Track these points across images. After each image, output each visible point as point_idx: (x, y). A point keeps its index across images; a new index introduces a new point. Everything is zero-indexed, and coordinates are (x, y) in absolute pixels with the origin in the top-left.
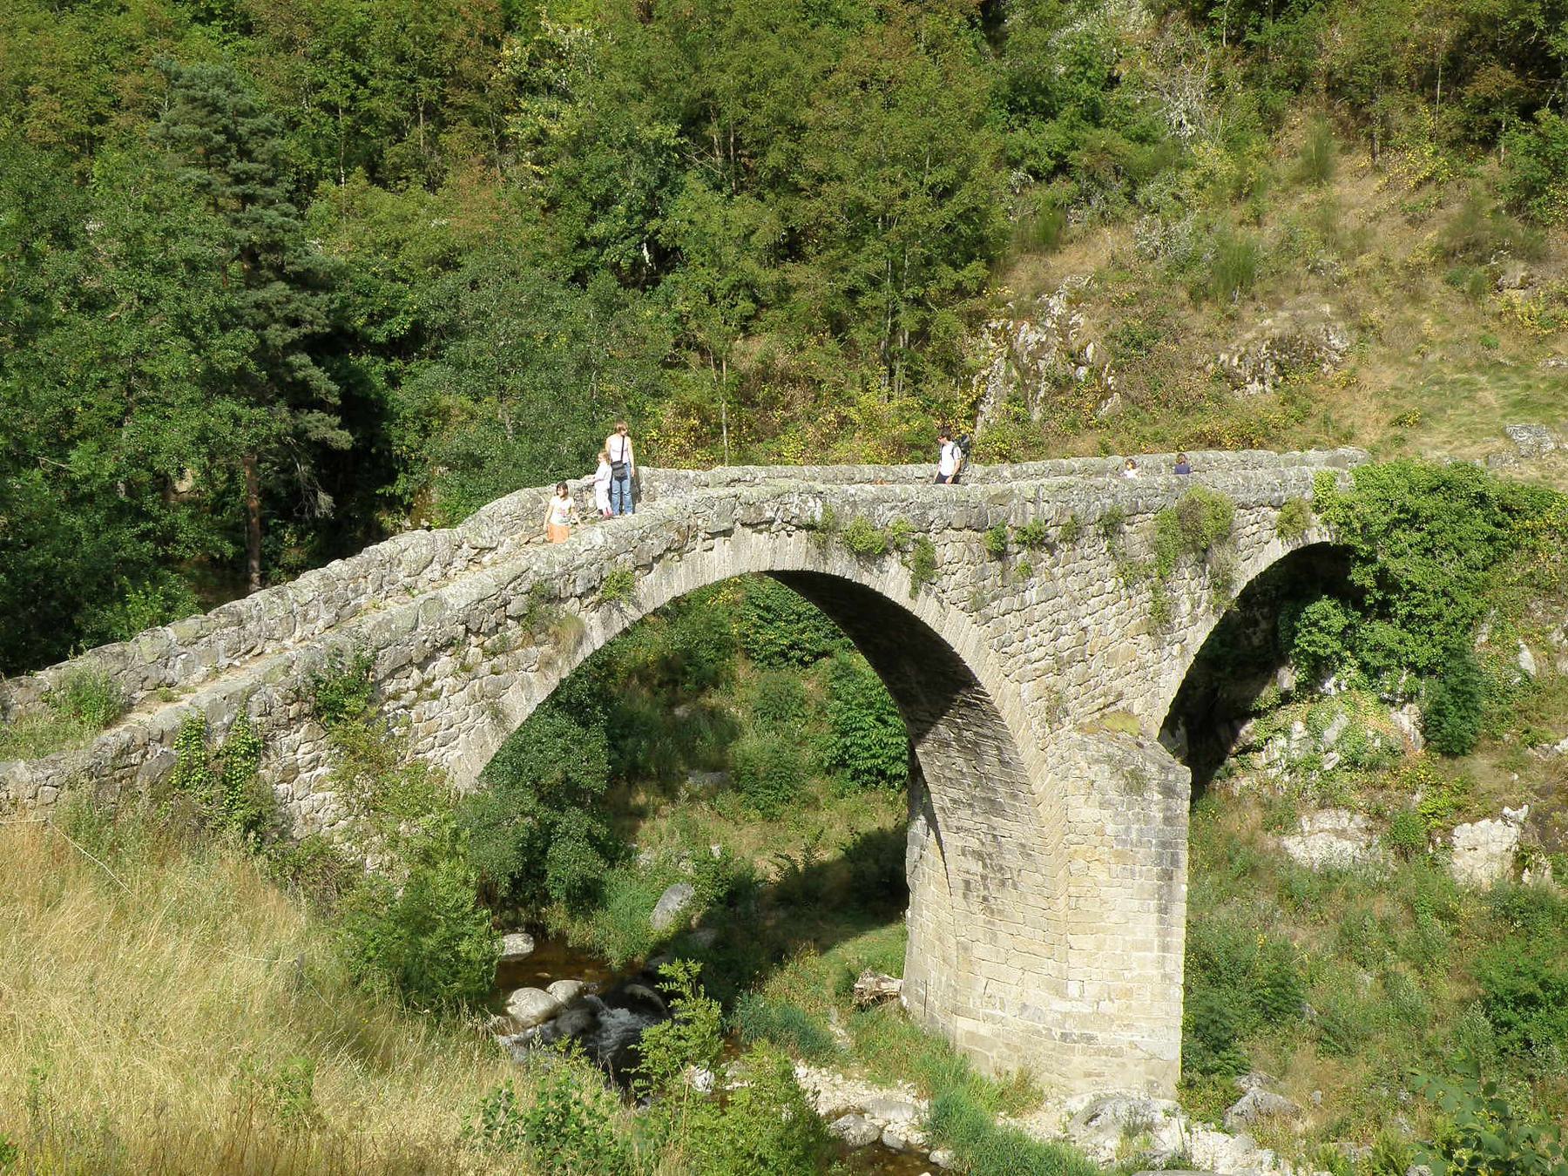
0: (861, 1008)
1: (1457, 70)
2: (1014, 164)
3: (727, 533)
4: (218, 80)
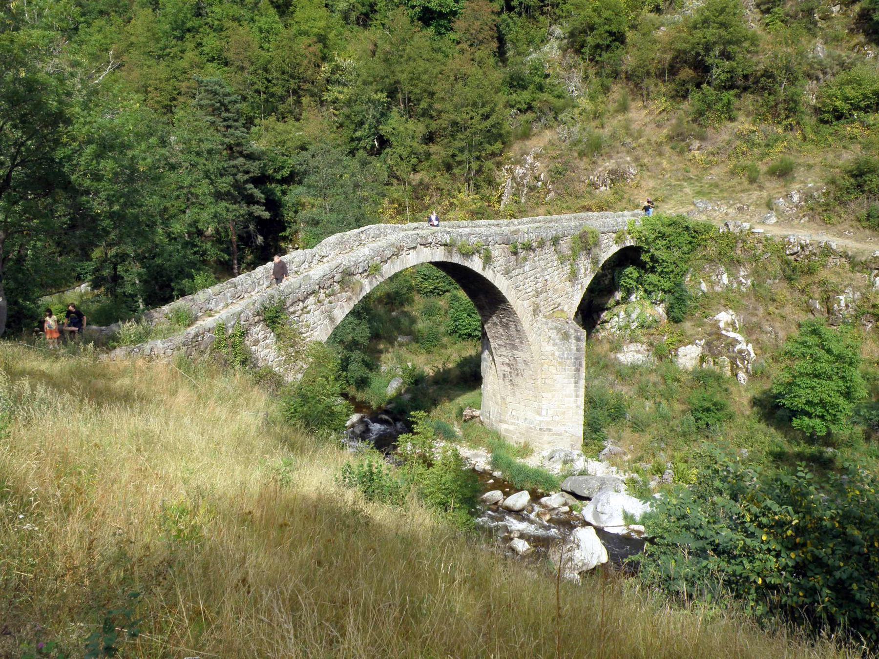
0: (465, 421)
1: (673, 70)
2: (512, 107)
3: (415, 248)
4: (216, 83)
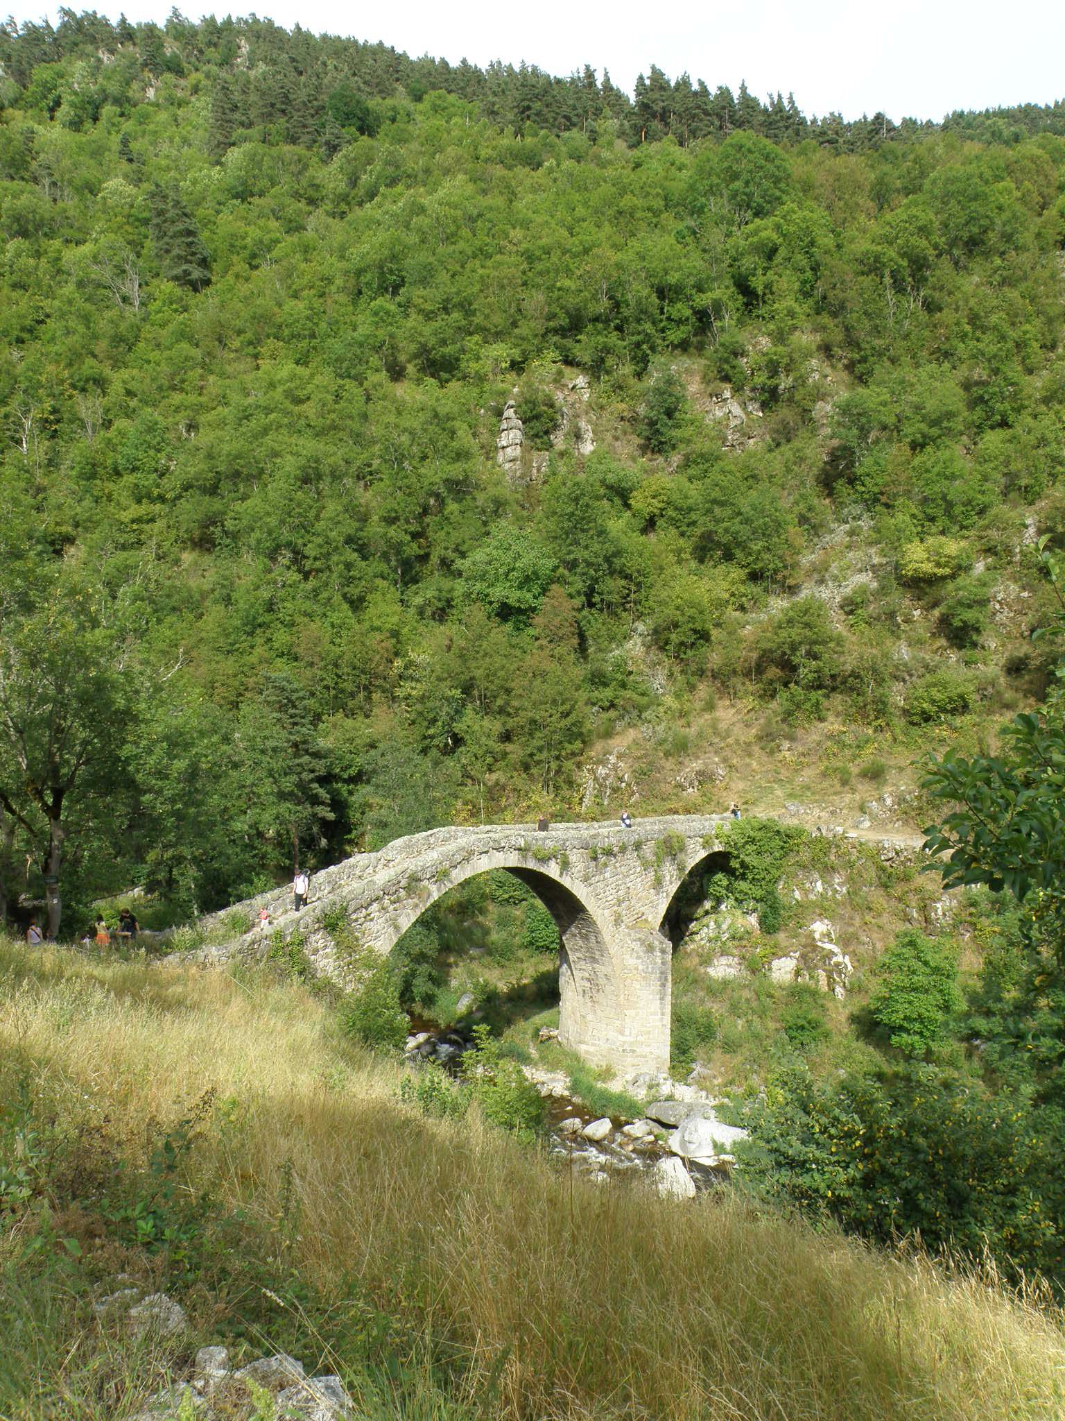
1: (760, 669)
2: (594, 704)
3: (486, 852)
4: (284, 679)
